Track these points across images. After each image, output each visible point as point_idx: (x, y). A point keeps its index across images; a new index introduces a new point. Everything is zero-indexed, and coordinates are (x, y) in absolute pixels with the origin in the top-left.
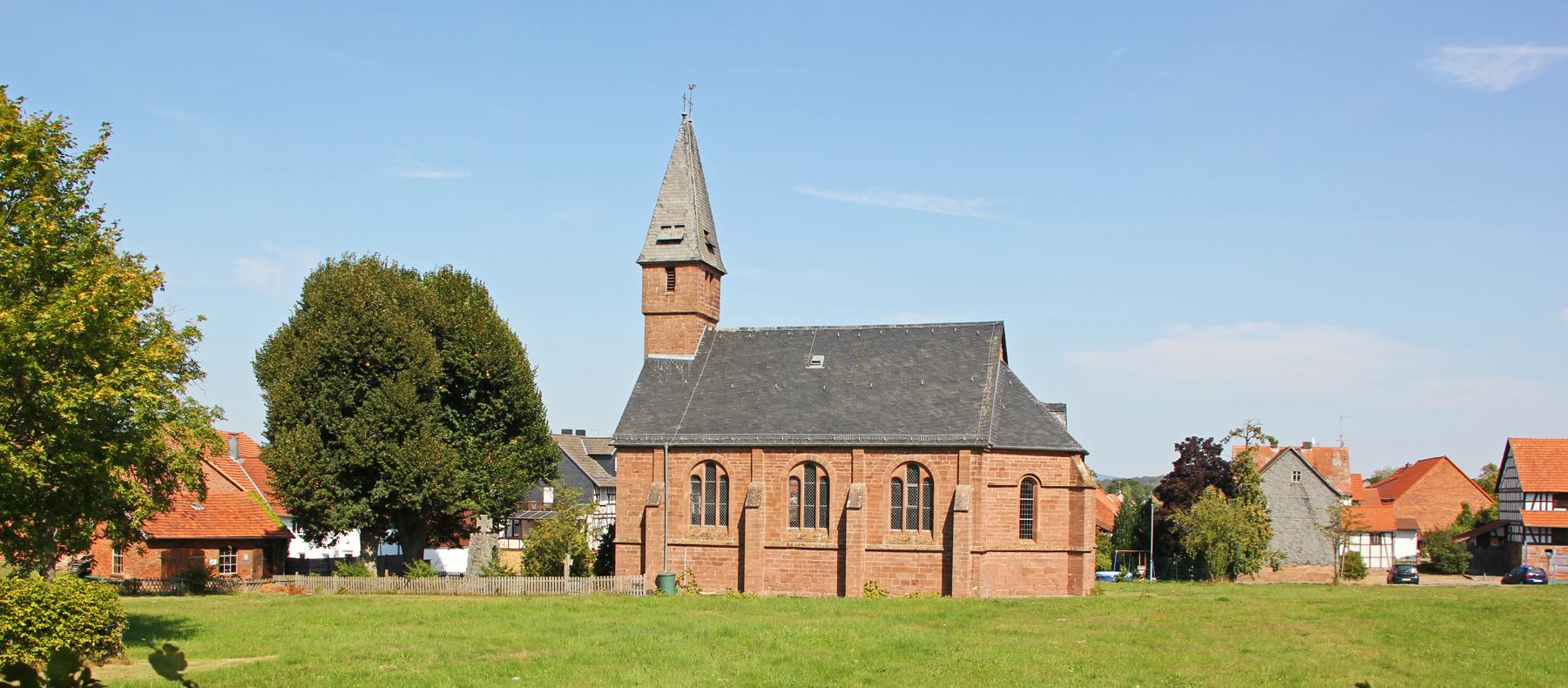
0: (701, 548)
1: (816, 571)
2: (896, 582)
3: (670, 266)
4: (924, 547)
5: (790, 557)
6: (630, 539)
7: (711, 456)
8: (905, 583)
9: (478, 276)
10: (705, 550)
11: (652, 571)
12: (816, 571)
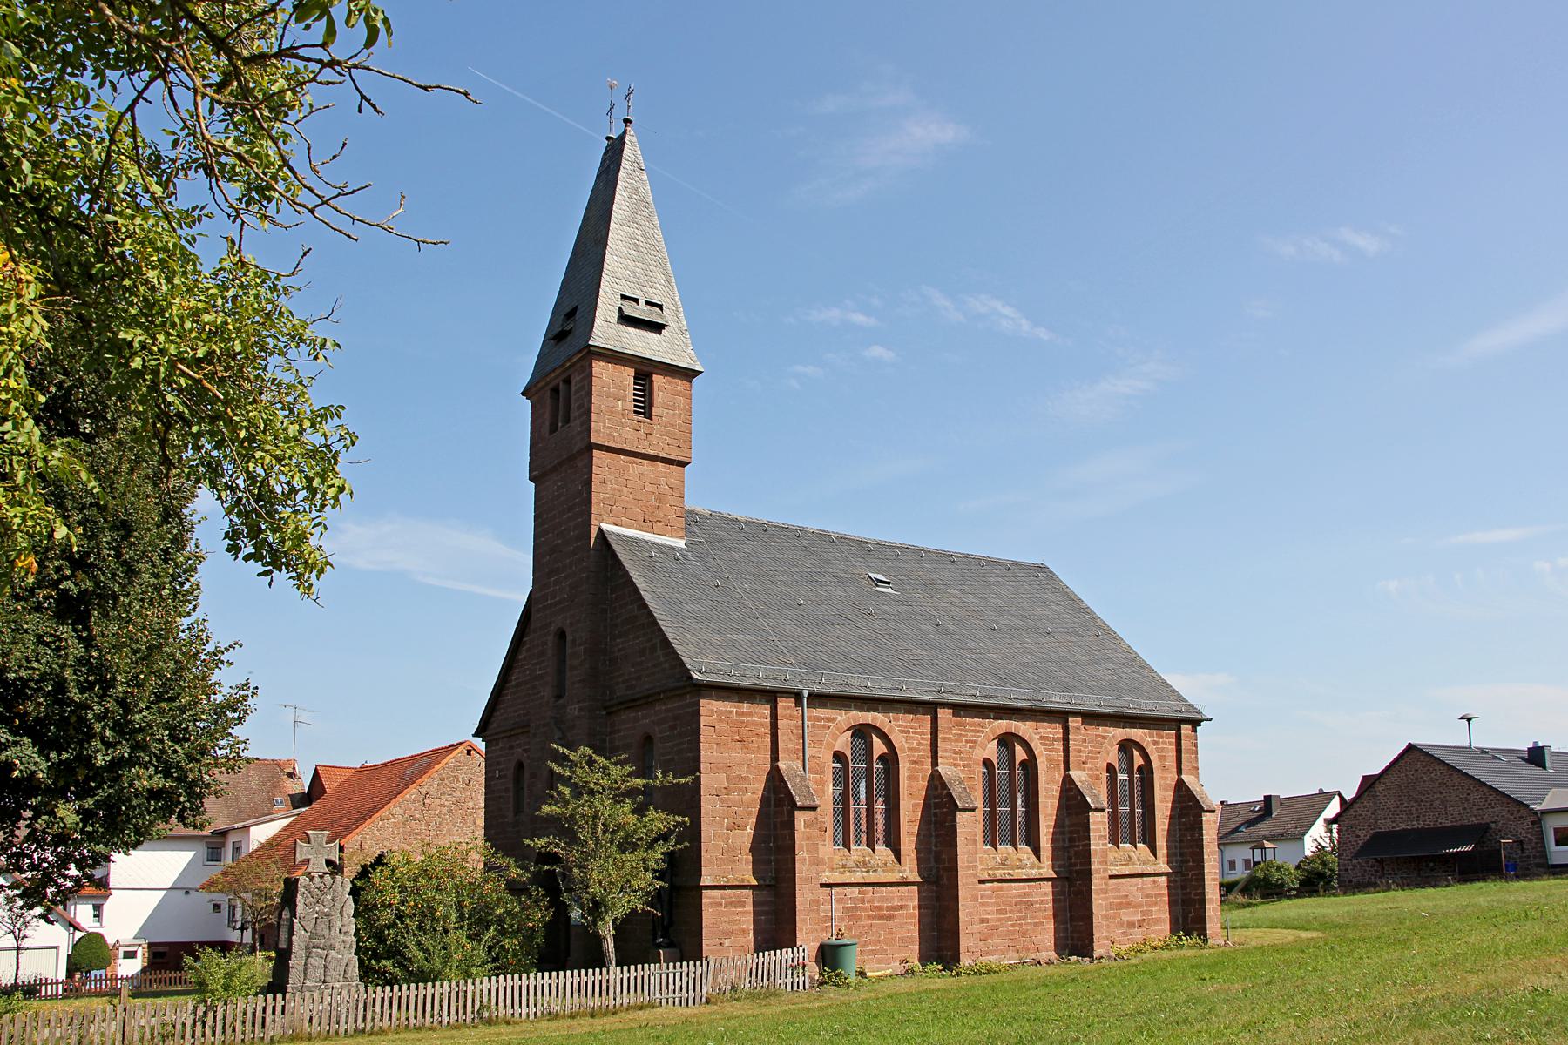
0: (856, 890)
1: (1025, 918)
2: (1121, 925)
3: (646, 369)
5: (990, 897)
6: (732, 879)
8: (1131, 925)
10: (865, 893)
11: (808, 940)
12: (1025, 918)
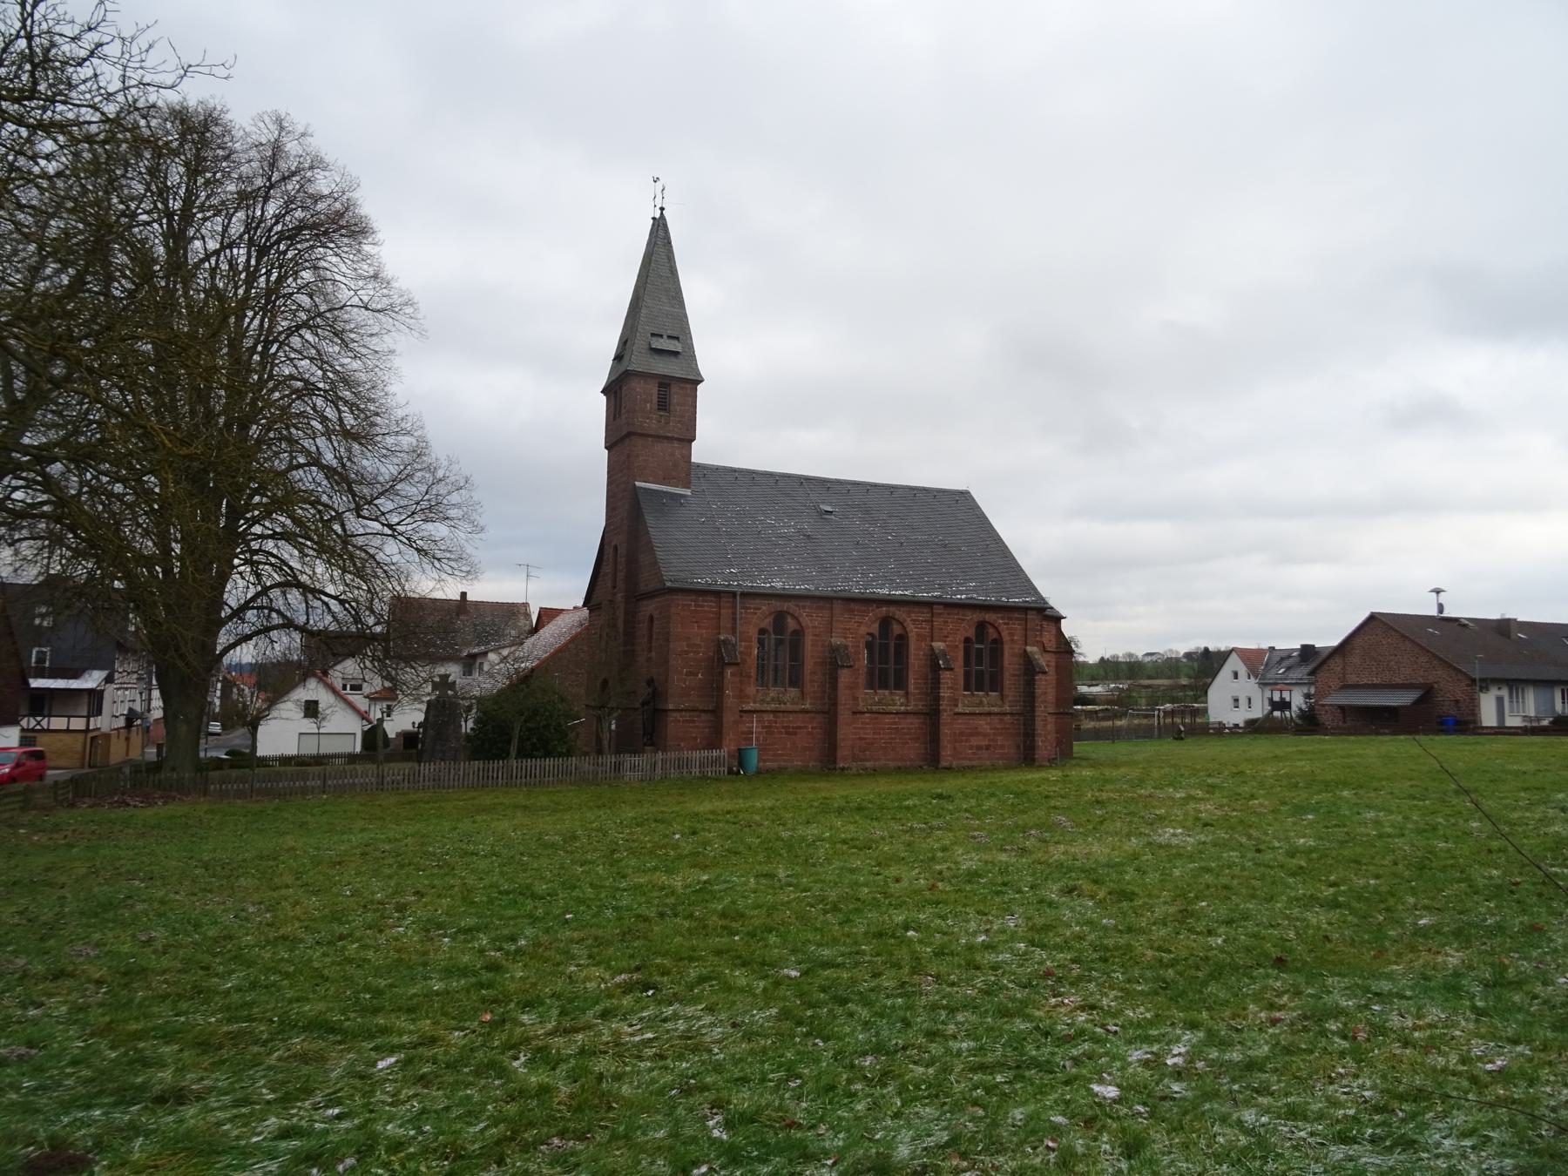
2: (971, 748)
4: (996, 709)
7: (785, 606)
9: (1133, 652)
